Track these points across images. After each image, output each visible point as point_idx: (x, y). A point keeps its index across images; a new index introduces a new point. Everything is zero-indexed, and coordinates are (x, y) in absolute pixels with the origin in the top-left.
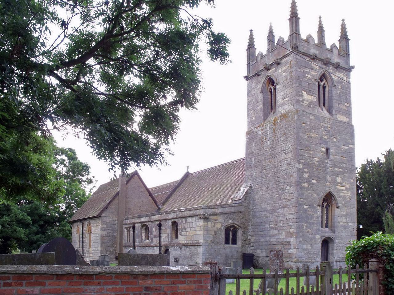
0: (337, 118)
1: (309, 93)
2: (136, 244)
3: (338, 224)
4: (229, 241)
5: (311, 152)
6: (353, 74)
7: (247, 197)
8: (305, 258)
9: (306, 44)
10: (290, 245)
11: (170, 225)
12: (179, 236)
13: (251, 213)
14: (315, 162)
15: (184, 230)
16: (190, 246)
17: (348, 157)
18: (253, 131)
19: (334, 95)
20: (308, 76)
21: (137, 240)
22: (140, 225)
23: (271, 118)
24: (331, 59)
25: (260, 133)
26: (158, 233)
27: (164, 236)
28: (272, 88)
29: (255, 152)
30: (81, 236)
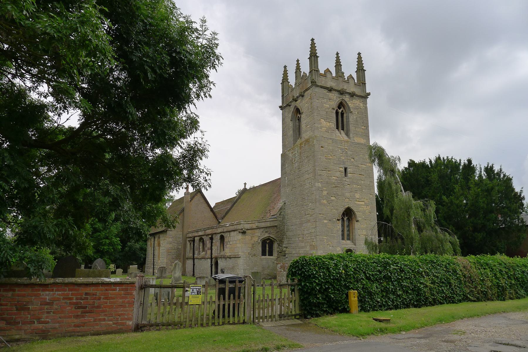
1: (327, 121)
2: (195, 256)
4: (266, 253)
6: (369, 100)
9: (323, 78)
15: (228, 243)
19: (350, 120)
20: (326, 105)
21: (196, 252)
23: (299, 141)
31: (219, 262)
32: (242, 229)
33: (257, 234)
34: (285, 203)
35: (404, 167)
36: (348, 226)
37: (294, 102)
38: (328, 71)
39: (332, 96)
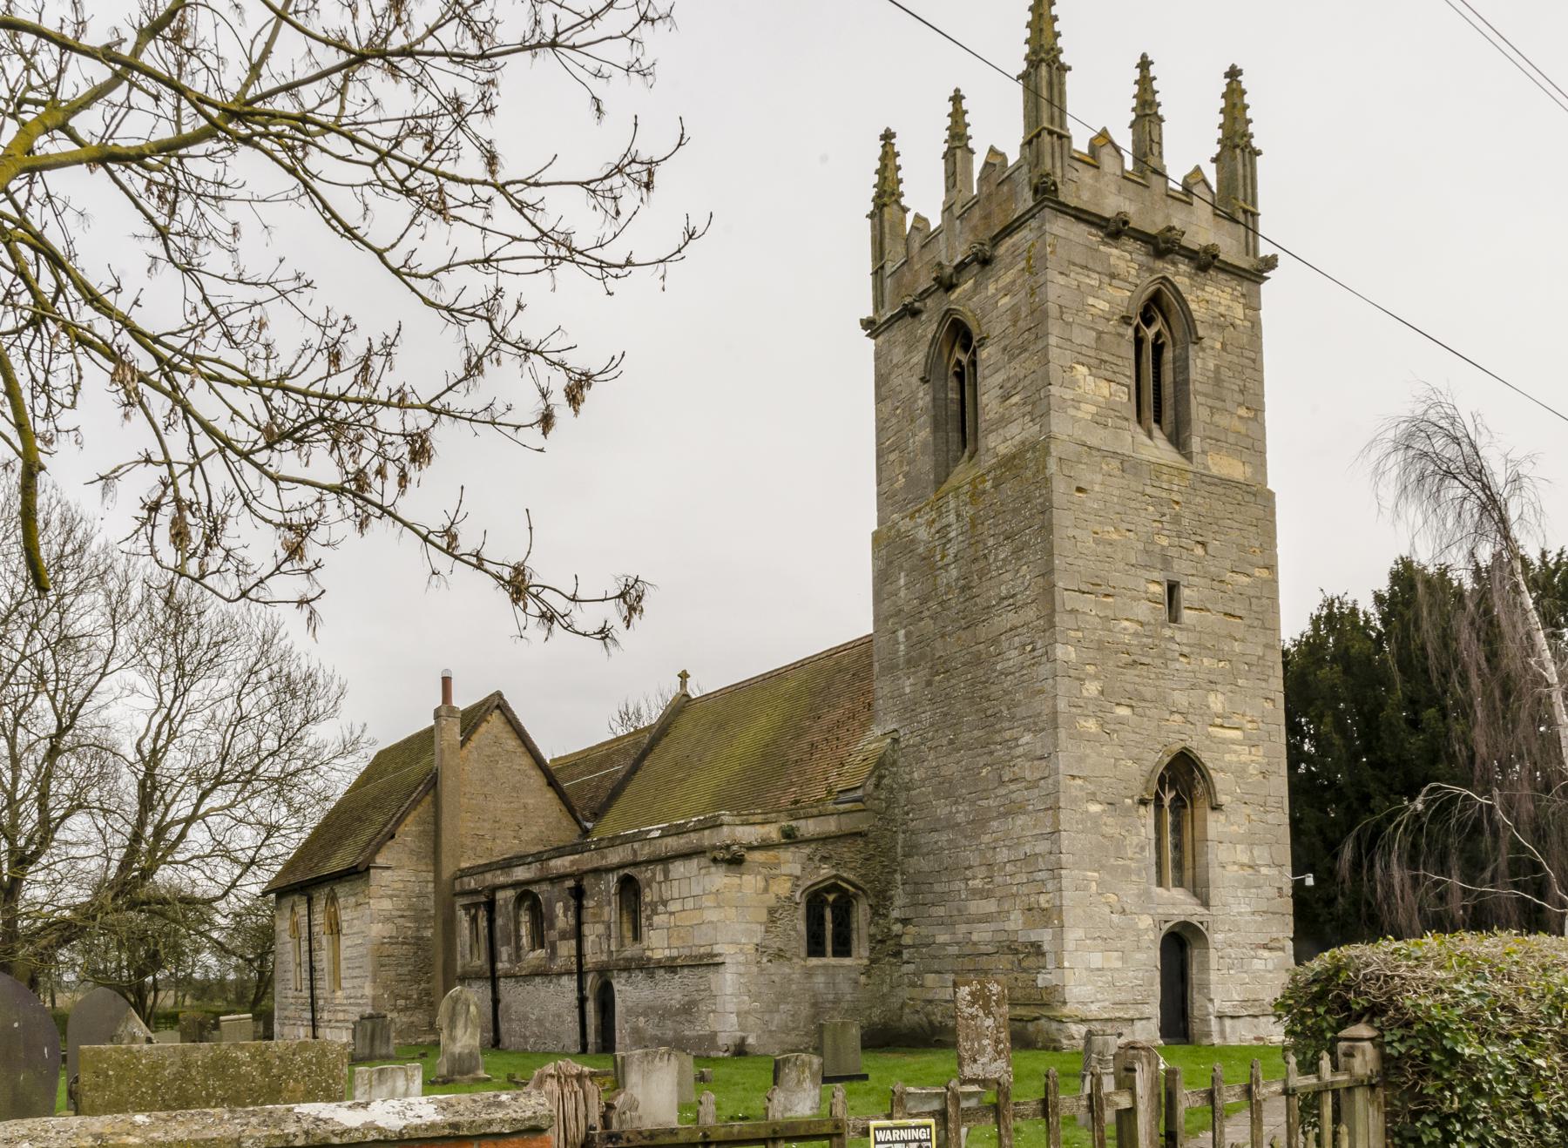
0: (1207, 467)
1: (1103, 373)
2: (500, 966)
3: (1219, 870)
5: (1110, 600)
6: (1269, 290)
7: (881, 777)
8: (1098, 1005)
9: (1087, 175)
10: (1044, 955)
11: (613, 891)
12: (644, 929)
13: (901, 836)
14: (1127, 639)
15: (661, 908)
16: (682, 967)
17: (1253, 615)
18: (899, 530)
19: (1194, 374)
21: (504, 952)
22: (510, 893)
23: (962, 474)
24: (1183, 233)
25: (923, 534)
26: (572, 921)
27: (591, 932)
28: (964, 359)
29: (906, 609)
30: (305, 945)
31: (616, 987)
32: (728, 847)
33: (785, 869)
34: (895, 741)
35: (1355, 602)
36: (1177, 829)
37: (940, 293)
38: (1103, 140)
39: (1122, 264)
